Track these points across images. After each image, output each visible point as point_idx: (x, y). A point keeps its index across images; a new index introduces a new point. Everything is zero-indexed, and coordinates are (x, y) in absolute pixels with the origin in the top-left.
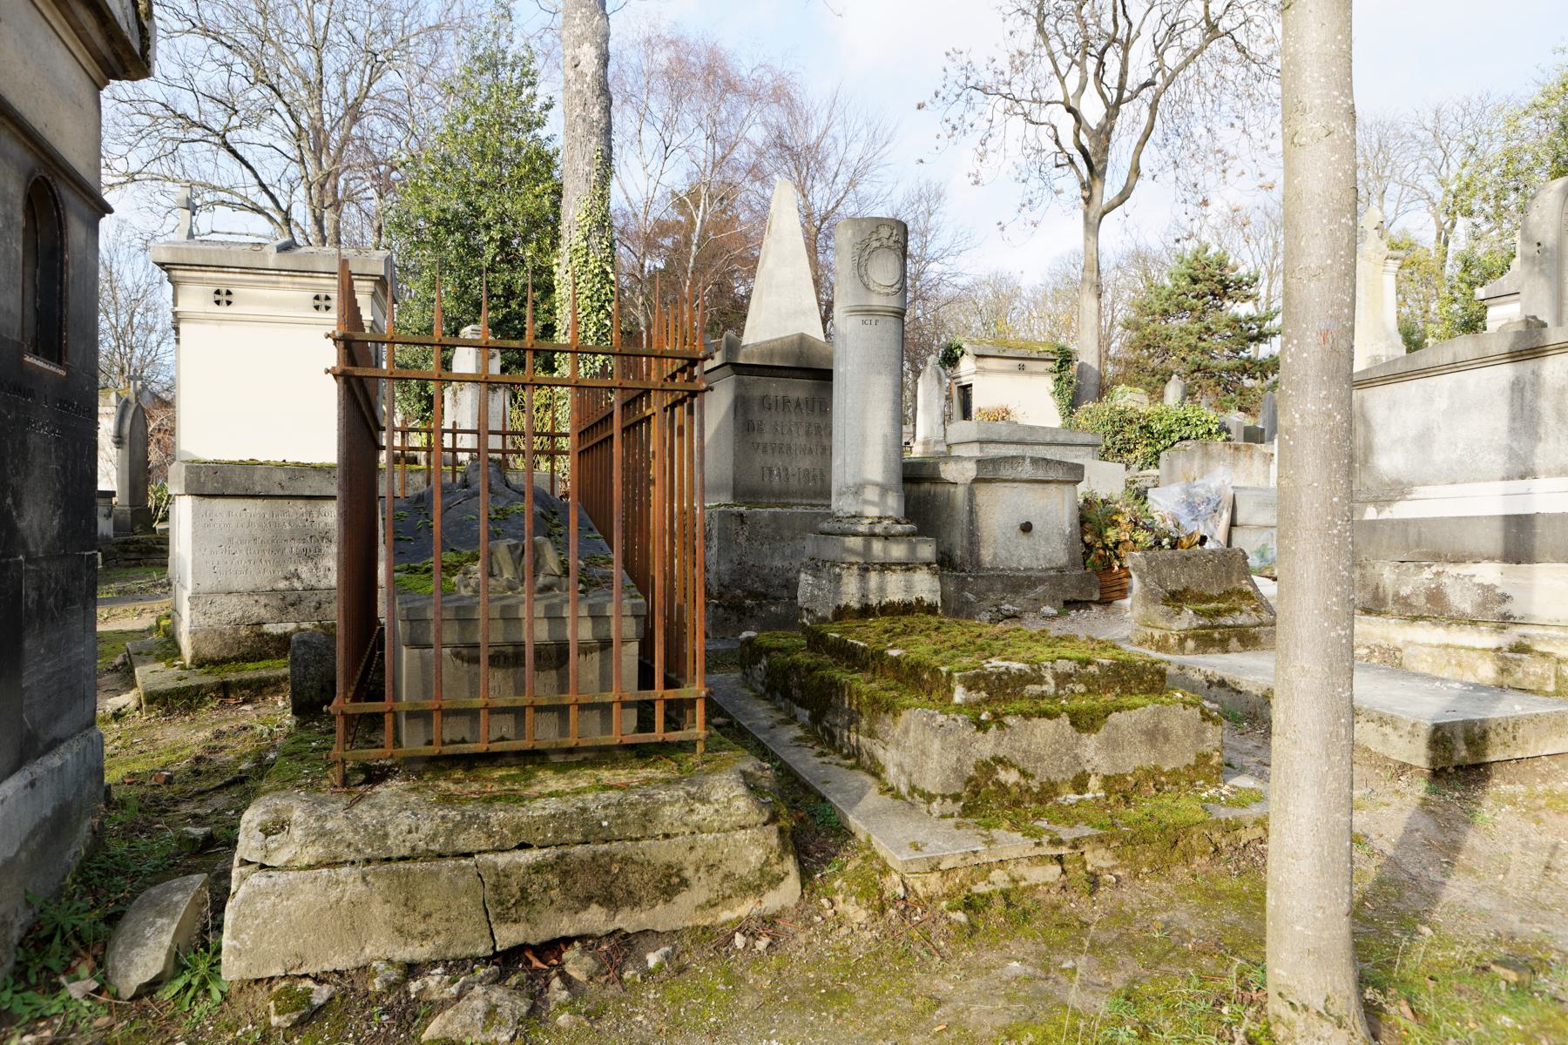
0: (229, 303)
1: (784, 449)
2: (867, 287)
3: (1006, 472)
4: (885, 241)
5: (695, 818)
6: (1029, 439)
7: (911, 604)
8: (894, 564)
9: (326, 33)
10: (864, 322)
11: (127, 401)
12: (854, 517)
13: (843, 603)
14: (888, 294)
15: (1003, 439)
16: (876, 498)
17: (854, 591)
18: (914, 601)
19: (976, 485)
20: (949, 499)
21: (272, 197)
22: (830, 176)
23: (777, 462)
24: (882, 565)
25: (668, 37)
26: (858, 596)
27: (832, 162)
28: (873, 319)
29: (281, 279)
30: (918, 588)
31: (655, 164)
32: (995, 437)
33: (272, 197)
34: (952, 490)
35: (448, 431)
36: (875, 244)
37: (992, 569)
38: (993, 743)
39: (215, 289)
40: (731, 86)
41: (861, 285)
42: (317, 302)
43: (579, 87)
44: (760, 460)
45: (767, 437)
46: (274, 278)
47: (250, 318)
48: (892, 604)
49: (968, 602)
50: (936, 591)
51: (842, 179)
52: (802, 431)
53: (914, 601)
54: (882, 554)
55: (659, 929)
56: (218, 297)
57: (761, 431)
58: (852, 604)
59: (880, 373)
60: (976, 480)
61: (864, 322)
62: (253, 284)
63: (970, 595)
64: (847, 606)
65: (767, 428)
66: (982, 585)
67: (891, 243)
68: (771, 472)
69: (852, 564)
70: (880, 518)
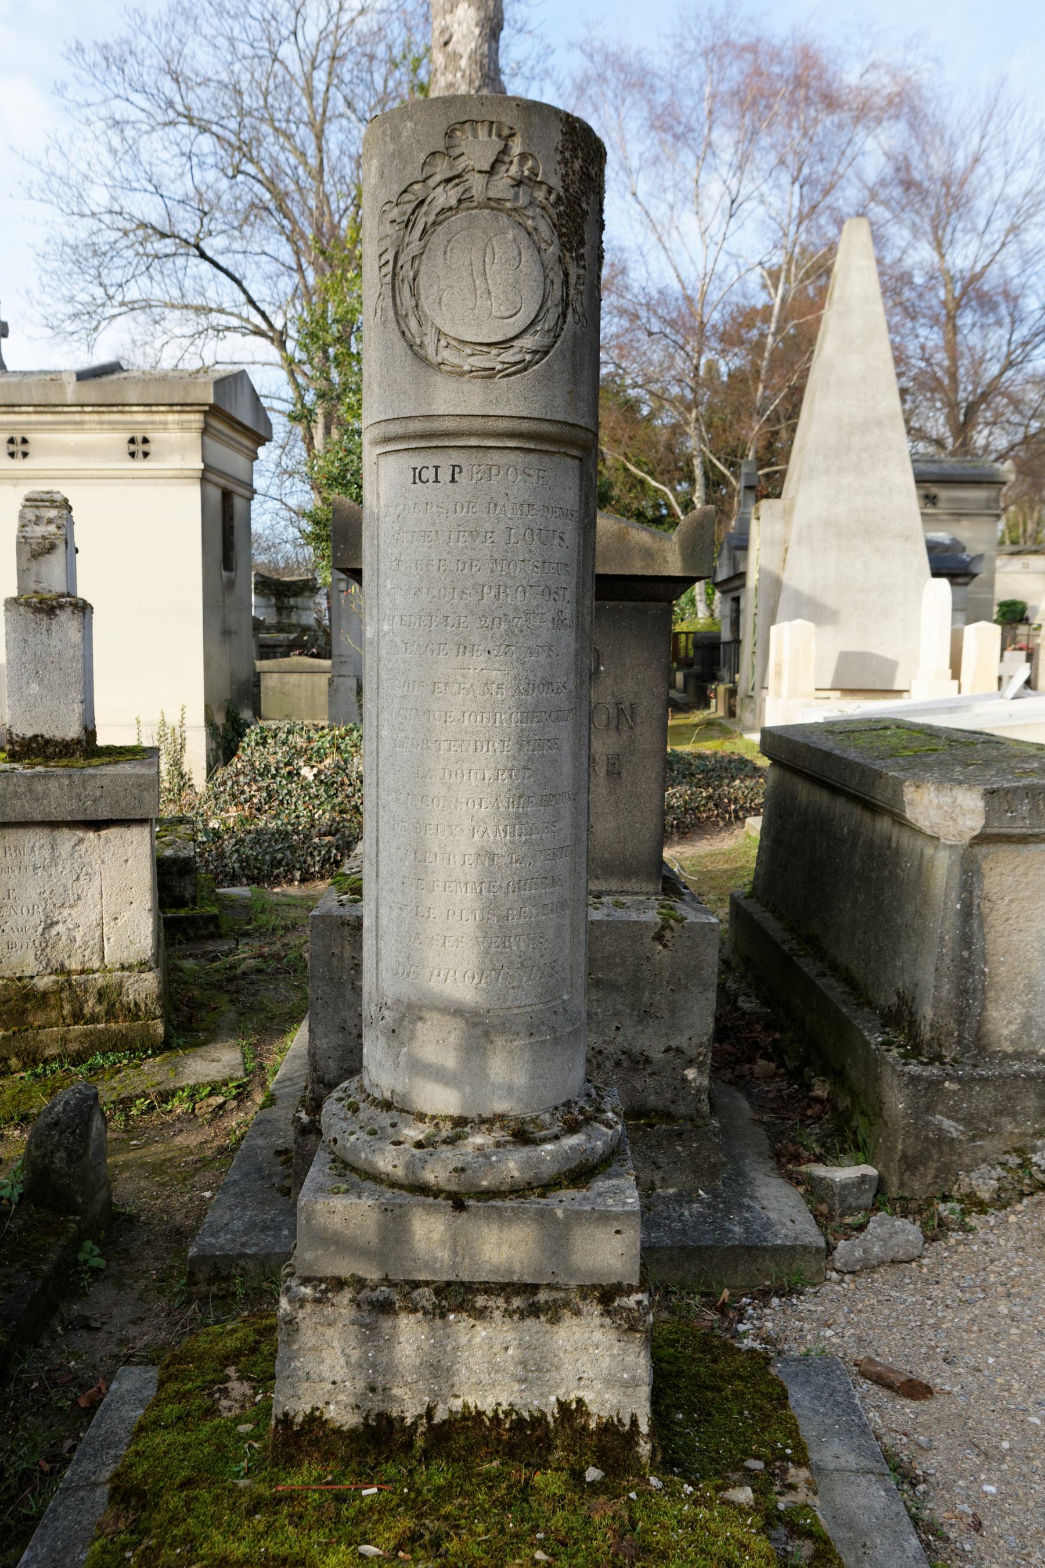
0: (25, 455)
2: (416, 351)
4: (476, 183)
7: (539, 1420)
8: (488, 1288)
9: (326, 100)
10: (418, 476)
12: (387, 1105)
13: (301, 1408)
14: (490, 373)
16: (450, 1060)
17: (341, 1373)
18: (551, 1410)
19: (984, 849)
20: (922, 871)
21: (263, 314)
22: (981, 224)
24: (442, 1290)
25: (743, 41)
26: (352, 1387)
27: (982, 204)
28: (445, 461)
29: (86, 417)
30: (568, 1370)
31: (716, 225)
33: (263, 314)
34: (929, 851)
36: (444, 197)
37: (1018, 1056)
39: (129, 436)
40: (831, 102)
41: (401, 346)
42: (133, 448)
43: (450, 77)
46: (77, 417)
47: (52, 473)
48: (472, 1418)
49: (942, 1140)
50: (633, 1383)
51: (1000, 225)
53: (551, 1410)
54: (444, 1255)
56: (12, 448)
58: (332, 1413)
59: (465, 647)
60: (982, 839)
62: (51, 427)
63: (948, 1124)
64: (314, 1419)
66: (984, 1099)
67: (501, 186)
69: (339, 1284)
70: (460, 1122)
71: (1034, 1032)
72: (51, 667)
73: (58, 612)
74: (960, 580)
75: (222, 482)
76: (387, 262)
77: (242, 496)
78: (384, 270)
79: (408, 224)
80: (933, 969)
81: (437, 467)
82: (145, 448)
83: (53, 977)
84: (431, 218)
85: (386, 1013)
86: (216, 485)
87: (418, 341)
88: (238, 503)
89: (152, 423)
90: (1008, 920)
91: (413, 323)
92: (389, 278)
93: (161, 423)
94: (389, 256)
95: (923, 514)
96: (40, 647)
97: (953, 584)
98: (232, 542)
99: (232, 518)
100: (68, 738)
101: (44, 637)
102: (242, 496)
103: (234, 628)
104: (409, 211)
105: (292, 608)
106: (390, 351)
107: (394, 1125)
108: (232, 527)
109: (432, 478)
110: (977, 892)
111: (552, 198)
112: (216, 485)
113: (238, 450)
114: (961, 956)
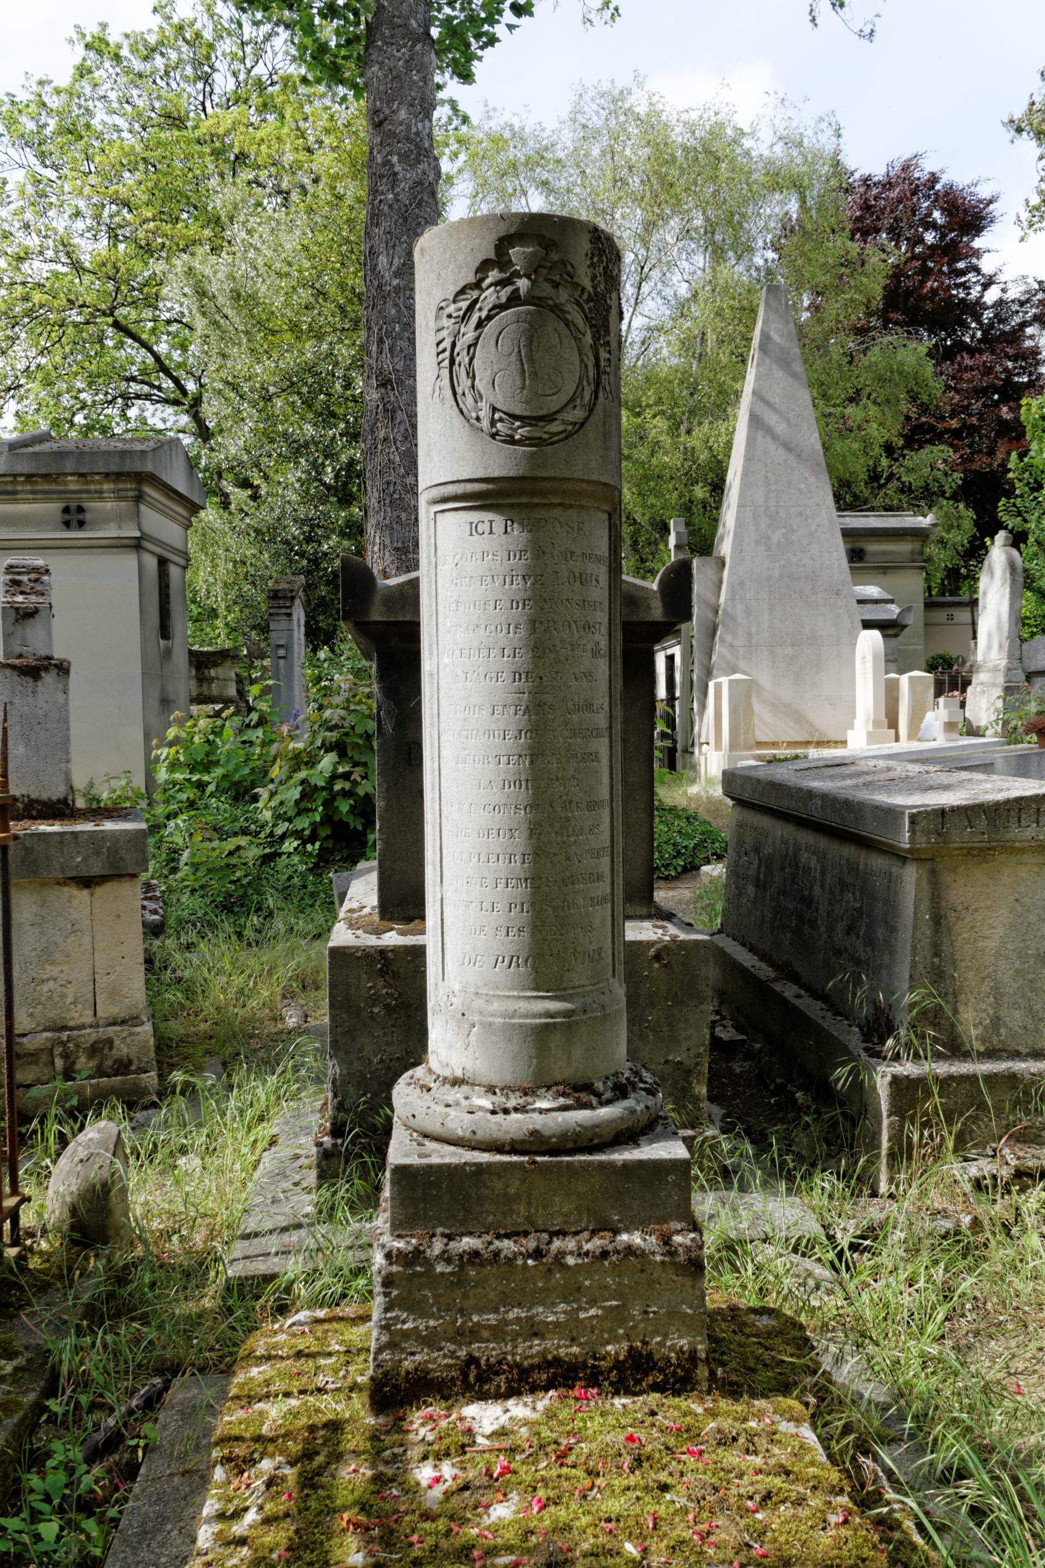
10: (474, 529)
47: (17, 544)
71: (1002, 1030)
72: (37, 728)
73: (43, 674)
74: (890, 632)
75: (158, 550)
76: (444, 350)
77: (177, 564)
78: (441, 357)
79: (465, 318)
80: (907, 977)
81: (491, 522)
82: (81, 517)
83: (49, 1034)
84: (484, 314)
85: (454, 1000)
86: (152, 553)
87: (474, 415)
88: (174, 571)
89: (88, 492)
90: (973, 927)
91: (469, 400)
92: (446, 363)
93: (96, 492)
94: (448, 344)
95: (851, 568)
96: (26, 709)
97: (884, 636)
98: (168, 610)
99: (168, 586)
100: (54, 798)
101: (30, 699)
102: (177, 564)
103: (172, 697)
104: (464, 308)
105: (213, 679)
106: (448, 424)
107: (467, 1098)
108: (168, 595)
109: (487, 531)
110: (944, 904)
111: (585, 297)
112: (152, 553)
113: (172, 519)
114: (933, 963)
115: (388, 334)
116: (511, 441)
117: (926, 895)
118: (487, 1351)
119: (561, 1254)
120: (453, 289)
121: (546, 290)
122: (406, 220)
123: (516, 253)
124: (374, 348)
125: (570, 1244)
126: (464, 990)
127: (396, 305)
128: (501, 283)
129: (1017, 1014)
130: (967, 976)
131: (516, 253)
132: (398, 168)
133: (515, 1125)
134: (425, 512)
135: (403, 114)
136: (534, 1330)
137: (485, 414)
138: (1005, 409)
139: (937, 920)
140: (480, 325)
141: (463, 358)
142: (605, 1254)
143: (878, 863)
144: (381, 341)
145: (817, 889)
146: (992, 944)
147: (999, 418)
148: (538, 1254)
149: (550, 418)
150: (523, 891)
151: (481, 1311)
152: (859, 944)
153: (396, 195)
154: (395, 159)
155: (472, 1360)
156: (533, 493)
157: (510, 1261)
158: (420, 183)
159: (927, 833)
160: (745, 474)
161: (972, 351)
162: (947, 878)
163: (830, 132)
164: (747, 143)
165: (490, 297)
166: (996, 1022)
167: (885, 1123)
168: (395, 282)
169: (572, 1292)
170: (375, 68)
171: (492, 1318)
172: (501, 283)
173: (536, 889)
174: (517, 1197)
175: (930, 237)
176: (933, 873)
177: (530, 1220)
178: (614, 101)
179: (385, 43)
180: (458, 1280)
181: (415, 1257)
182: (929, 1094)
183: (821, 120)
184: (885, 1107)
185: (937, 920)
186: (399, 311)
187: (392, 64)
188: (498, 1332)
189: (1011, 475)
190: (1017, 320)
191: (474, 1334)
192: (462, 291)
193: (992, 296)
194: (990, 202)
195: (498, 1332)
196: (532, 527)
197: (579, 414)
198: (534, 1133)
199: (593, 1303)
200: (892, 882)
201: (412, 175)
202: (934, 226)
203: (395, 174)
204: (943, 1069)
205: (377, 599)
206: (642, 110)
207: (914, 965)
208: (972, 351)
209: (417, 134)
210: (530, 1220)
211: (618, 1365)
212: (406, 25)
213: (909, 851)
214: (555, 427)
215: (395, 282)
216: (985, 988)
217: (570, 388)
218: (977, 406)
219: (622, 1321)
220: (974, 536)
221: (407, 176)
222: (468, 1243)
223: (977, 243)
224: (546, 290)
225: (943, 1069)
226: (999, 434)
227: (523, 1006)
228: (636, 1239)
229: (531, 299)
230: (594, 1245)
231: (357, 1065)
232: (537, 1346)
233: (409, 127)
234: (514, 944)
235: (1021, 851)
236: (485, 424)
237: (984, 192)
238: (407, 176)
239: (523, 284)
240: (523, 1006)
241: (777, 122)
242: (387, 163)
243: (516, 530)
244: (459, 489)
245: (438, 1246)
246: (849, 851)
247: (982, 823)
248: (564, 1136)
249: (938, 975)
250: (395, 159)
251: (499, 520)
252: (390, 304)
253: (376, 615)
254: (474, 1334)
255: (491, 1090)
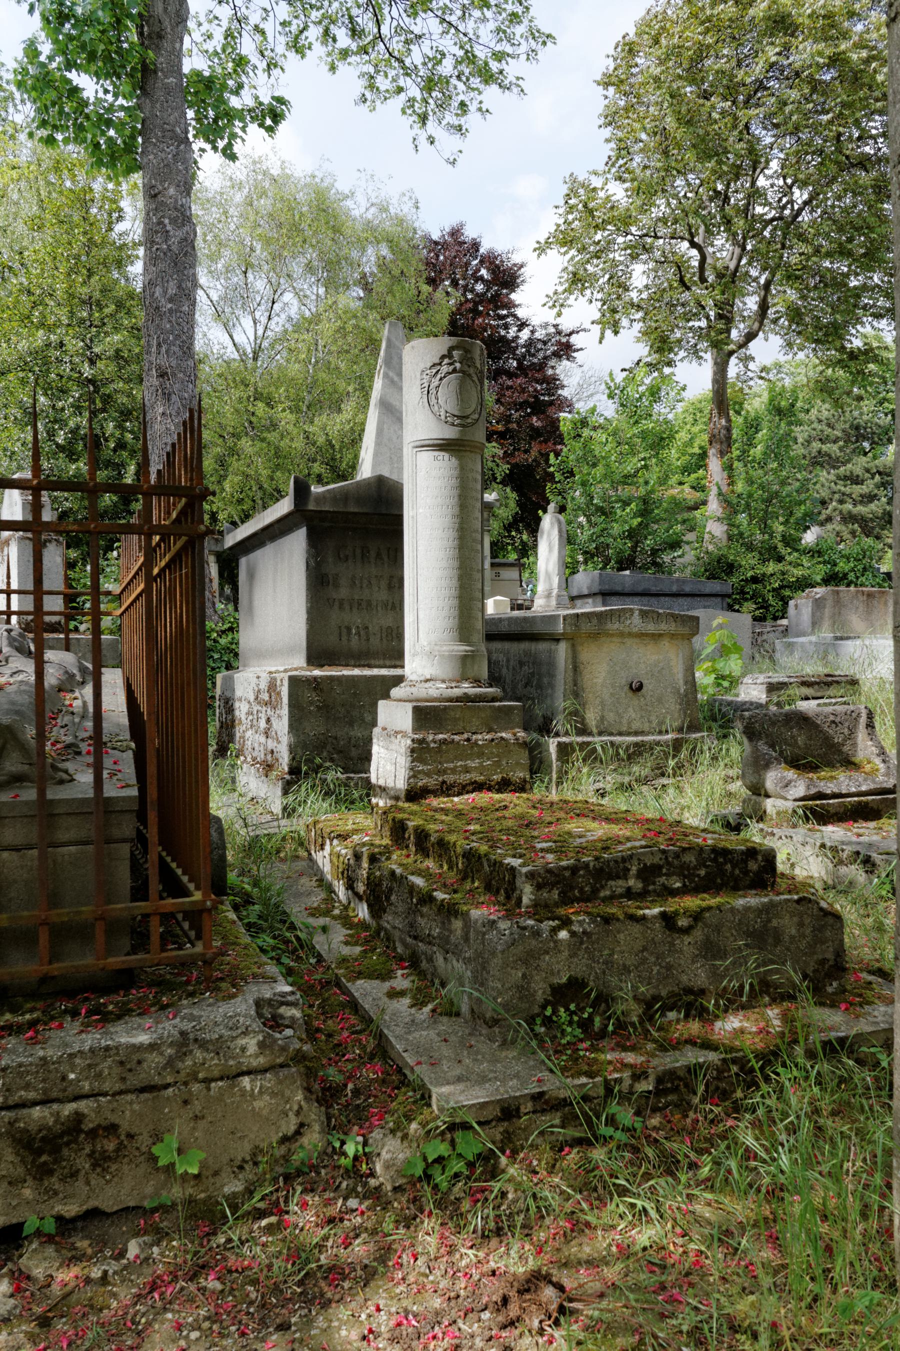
1: (364, 605)
3: (614, 626)
5: (183, 1074)
6: (654, 589)
10: (435, 458)
11: (529, 608)
15: (626, 590)
23: (356, 619)
32: (619, 588)
35: (15, 592)
38: (566, 953)
44: (336, 618)
45: (343, 592)
52: (384, 584)
55: (147, 1204)
57: (336, 586)
61: (435, 458)
65: (344, 582)
68: (349, 629)
91: (436, 408)
94: (426, 385)
115: (165, 341)
116: (453, 425)
117: (570, 656)
118: (450, 778)
119: (477, 740)
120: (429, 364)
121: (466, 368)
122: (176, 264)
123: (455, 353)
124: (154, 349)
125: (480, 737)
126: (429, 644)
127: (170, 322)
128: (450, 364)
129: (611, 714)
130: (588, 696)
131: (455, 353)
132: (169, 228)
133: (457, 692)
134: (408, 451)
135: (172, 191)
136: (467, 770)
137: (443, 413)
138: (535, 419)
139: (575, 669)
140: (441, 379)
141: (433, 391)
142: (493, 740)
143: (542, 646)
144: (159, 345)
145: (504, 671)
146: (600, 681)
147: (532, 426)
148: (468, 740)
149: (467, 417)
150: (456, 602)
151: (447, 762)
152: (533, 690)
153: (169, 246)
154: (167, 221)
155: (444, 782)
156: (460, 446)
157: (458, 743)
158: (186, 240)
159: (571, 625)
160: (376, 455)
161: (510, 375)
162: (579, 648)
163: (410, 204)
164: (349, 203)
165: (445, 369)
166: (602, 718)
167: (554, 765)
168: (169, 306)
169: (481, 755)
170: (151, 157)
171: (451, 765)
172: (450, 364)
173: (460, 602)
174: (459, 719)
175: (480, 287)
176: (573, 646)
177: (464, 728)
178: (254, 163)
179: (158, 140)
180: (439, 750)
181: (421, 741)
182: (574, 751)
183: (404, 195)
184: (554, 756)
185: (575, 669)
186: (172, 326)
187: (163, 155)
188: (454, 771)
189: (552, 469)
190: (541, 355)
191: (444, 772)
192: (434, 365)
193: (525, 335)
194: (522, 266)
195: (454, 771)
196: (459, 458)
197: (476, 416)
198: (465, 694)
199: (488, 759)
200: (552, 655)
201: (180, 234)
202: (481, 278)
203: (167, 232)
204: (580, 739)
205: (312, 498)
206: (275, 172)
207: (565, 689)
208: (510, 375)
209: (182, 206)
210: (464, 728)
211: (498, 783)
212: (173, 131)
213: (562, 634)
214: (469, 421)
215: (169, 306)
216: (597, 702)
217: (474, 406)
218: (516, 415)
219: (499, 766)
220: (517, 513)
221: (176, 235)
222: (441, 736)
223: (513, 296)
224: (466, 368)
225: (580, 739)
226: (532, 438)
227: (456, 648)
228: (504, 735)
229: (461, 371)
230: (488, 737)
231: (302, 737)
232: (468, 776)
233: (176, 201)
234: (453, 623)
235: (612, 635)
236: (443, 417)
237: (516, 259)
238: (176, 235)
239: (458, 365)
240: (456, 648)
241: (369, 191)
242: (160, 223)
243: (454, 459)
244: (431, 442)
245: (431, 737)
246: (525, 646)
247: (595, 621)
248: (476, 695)
249: (576, 695)
250: (167, 221)
251: (446, 455)
252: (165, 321)
253: (311, 506)
254: (444, 772)
255: (443, 681)
